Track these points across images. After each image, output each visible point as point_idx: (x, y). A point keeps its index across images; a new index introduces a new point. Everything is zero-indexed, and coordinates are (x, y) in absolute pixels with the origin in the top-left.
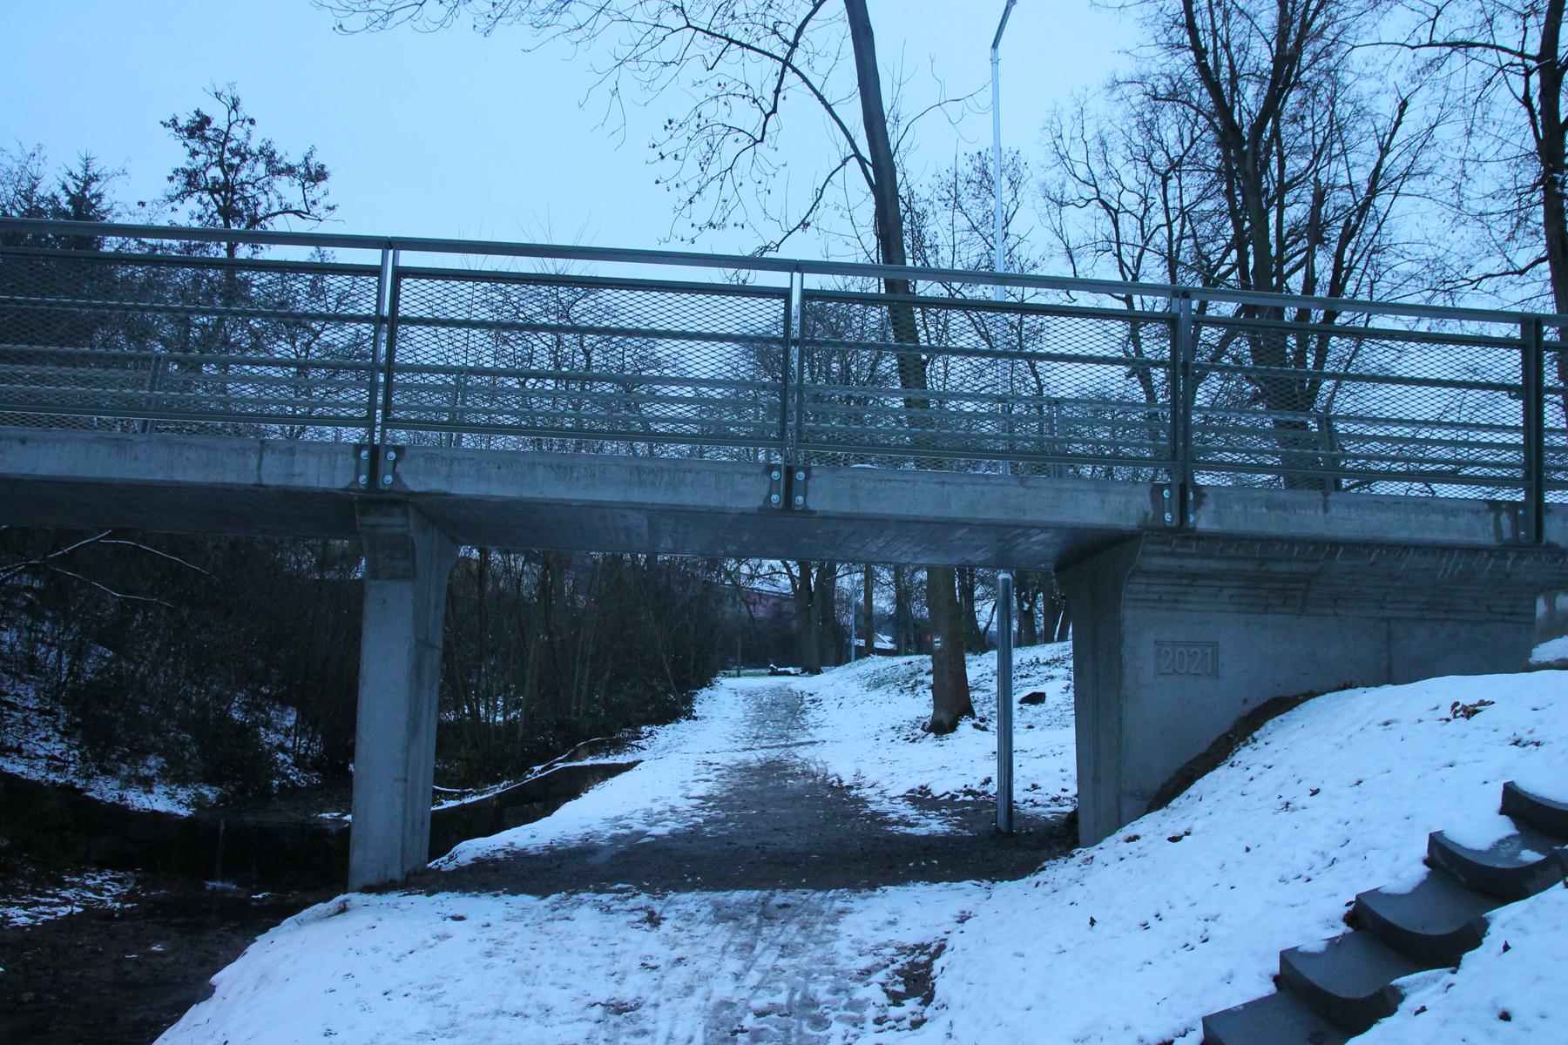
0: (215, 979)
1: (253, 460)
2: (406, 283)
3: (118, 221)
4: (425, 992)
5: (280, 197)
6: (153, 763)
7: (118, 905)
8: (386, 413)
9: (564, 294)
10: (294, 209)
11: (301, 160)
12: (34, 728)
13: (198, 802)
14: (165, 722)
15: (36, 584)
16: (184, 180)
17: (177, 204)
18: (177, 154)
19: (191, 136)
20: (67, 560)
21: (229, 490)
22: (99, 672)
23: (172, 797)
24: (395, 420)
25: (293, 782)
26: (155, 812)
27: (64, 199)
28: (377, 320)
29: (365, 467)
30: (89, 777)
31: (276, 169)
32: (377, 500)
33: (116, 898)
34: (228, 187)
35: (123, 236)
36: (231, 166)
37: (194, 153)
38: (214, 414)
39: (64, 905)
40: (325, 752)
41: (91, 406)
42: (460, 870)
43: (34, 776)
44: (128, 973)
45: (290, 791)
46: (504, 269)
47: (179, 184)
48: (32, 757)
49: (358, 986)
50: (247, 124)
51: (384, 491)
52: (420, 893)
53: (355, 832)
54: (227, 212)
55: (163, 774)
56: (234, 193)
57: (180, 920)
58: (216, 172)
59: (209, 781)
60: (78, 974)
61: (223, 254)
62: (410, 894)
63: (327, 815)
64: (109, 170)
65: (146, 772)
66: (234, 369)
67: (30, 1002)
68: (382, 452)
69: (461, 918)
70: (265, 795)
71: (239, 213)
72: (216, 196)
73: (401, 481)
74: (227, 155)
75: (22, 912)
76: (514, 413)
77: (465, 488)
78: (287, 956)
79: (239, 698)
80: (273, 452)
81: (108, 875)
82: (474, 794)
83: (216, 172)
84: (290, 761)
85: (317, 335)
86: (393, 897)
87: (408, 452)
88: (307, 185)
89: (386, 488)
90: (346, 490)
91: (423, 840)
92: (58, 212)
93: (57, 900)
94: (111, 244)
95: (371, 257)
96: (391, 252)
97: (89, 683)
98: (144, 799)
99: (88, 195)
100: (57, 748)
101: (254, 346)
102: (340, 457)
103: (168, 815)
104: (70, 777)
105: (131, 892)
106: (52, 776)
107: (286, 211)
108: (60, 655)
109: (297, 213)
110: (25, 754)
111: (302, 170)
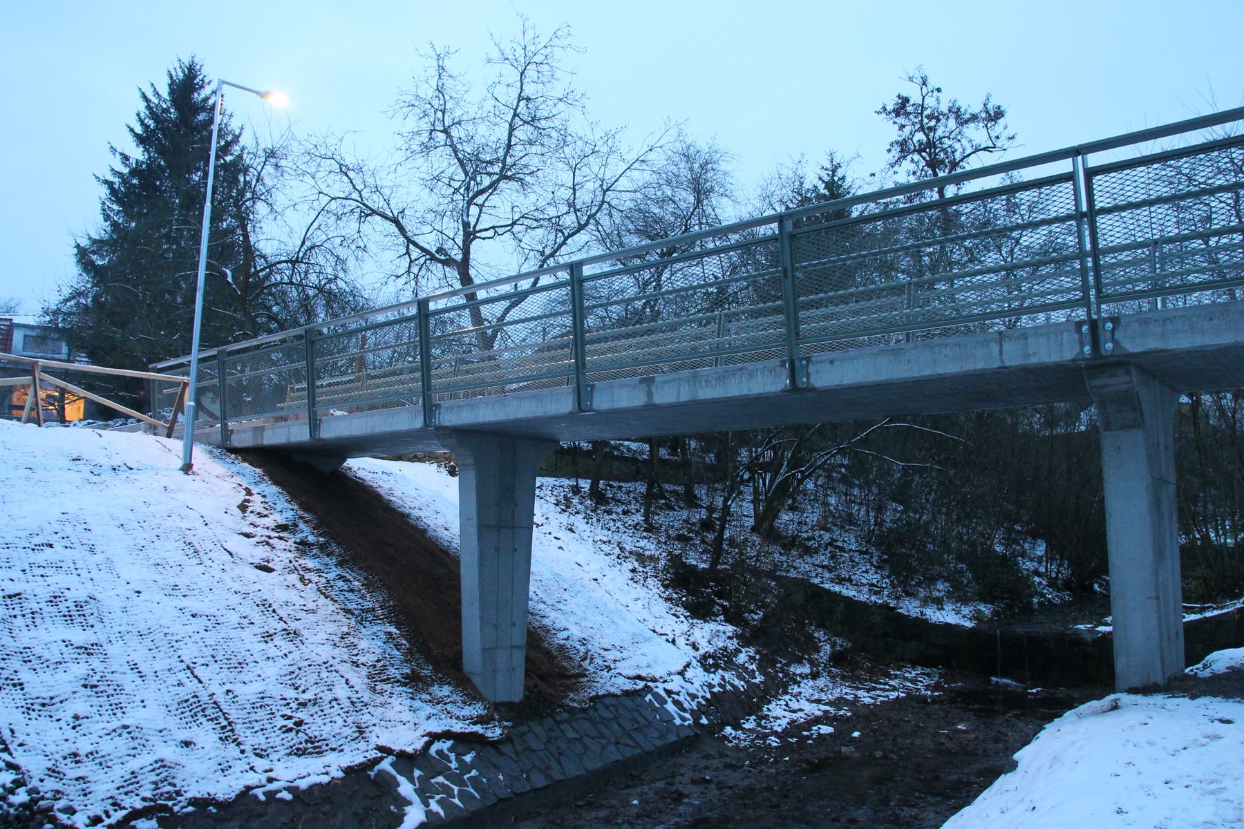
0: (1017, 756)
1: (995, 348)
2: (1098, 180)
3: (860, 192)
4: (1205, 786)
5: (970, 141)
6: (941, 587)
7: (929, 693)
8: (1099, 291)
9: (1184, 164)
10: (982, 147)
11: (981, 107)
12: (858, 564)
13: (978, 616)
14: (946, 556)
15: (846, 462)
16: (899, 149)
17: (896, 168)
18: (890, 131)
19: (898, 115)
20: (864, 441)
21: (981, 375)
22: (895, 522)
23: (958, 613)
24: (1107, 296)
25: (1049, 599)
26: (947, 624)
27: (821, 186)
28: (1078, 216)
29: (1088, 339)
30: (898, 598)
31: (963, 120)
32: (1100, 365)
33: (927, 687)
34: (930, 145)
35: (1006, 171)
36: (930, 128)
37: (902, 127)
38: (949, 320)
39: (892, 690)
40: (1072, 575)
41: (861, 331)
42: (1215, 678)
43: (863, 598)
44: (942, 744)
45: (1046, 607)
46: (1182, 146)
47: (896, 152)
48: (859, 585)
49: (1139, 773)
50: (936, 92)
51: (1106, 357)
52: (1184, 696)
53: (1116, 642)
54: (933, 164)
55: (949, 595)
56: (935, 148)
57: (976, 706)
58: (920, 136)
59: (984, 600)
60: (908, 741)
61: (936, 196)
62: (1174, 697)
63: (1082, 627)
64: (848, 157)
65: (938, 594)
66: (958, 283)
67: (880, 758)
68: (1100, 325)
69: (1229, 722)
70: (1028, 610)
71: (942, 162)
72: (923, 154)
73: (1120, 346)
74: (925, 121)
75: (866, 694)
76: (1203, 270)
77: (1180, 342)
78: (1074, 742)
79: (999, 535)
80: (1010, 340)
81: (919, 671)
82: (1214, 609)
83: (920, 136)
84: (1044, 583)
85: (1017, 242)
86: (1159, 699)
87: (1123, 321)
88: (989, 125)
89: (1109, 353)
90: (1073, 360)
91: (1178, 649)
92: (820, 197)
93: (887, 687)
94: (856, 211)
95: (1064, 166)
96: (1080, 158)
97: (890, 530)
98: (938, 613)
99: (836, 179)
100: (874, 578)
101: (970, 261)
102: (1065, 335)
103: (957, 626)
104: (886, 599)
105: (937, 683)
106: (873, 598)
107: (977, 150)
108: (868, 511)
109: (985, 149)
110: (854, 582)
111: (983, 115)
